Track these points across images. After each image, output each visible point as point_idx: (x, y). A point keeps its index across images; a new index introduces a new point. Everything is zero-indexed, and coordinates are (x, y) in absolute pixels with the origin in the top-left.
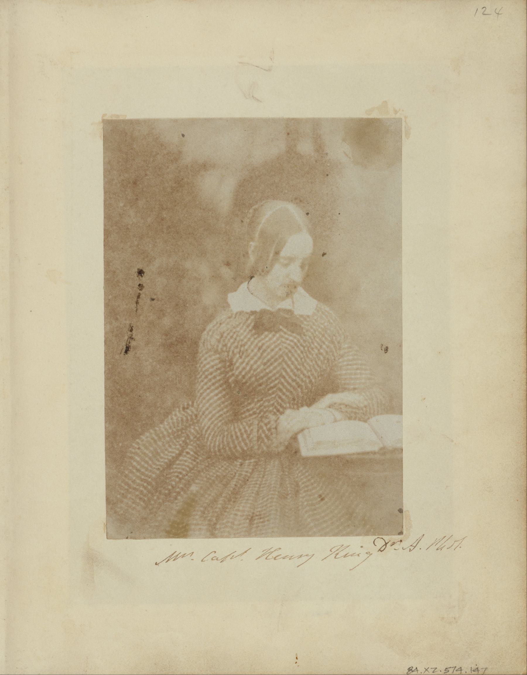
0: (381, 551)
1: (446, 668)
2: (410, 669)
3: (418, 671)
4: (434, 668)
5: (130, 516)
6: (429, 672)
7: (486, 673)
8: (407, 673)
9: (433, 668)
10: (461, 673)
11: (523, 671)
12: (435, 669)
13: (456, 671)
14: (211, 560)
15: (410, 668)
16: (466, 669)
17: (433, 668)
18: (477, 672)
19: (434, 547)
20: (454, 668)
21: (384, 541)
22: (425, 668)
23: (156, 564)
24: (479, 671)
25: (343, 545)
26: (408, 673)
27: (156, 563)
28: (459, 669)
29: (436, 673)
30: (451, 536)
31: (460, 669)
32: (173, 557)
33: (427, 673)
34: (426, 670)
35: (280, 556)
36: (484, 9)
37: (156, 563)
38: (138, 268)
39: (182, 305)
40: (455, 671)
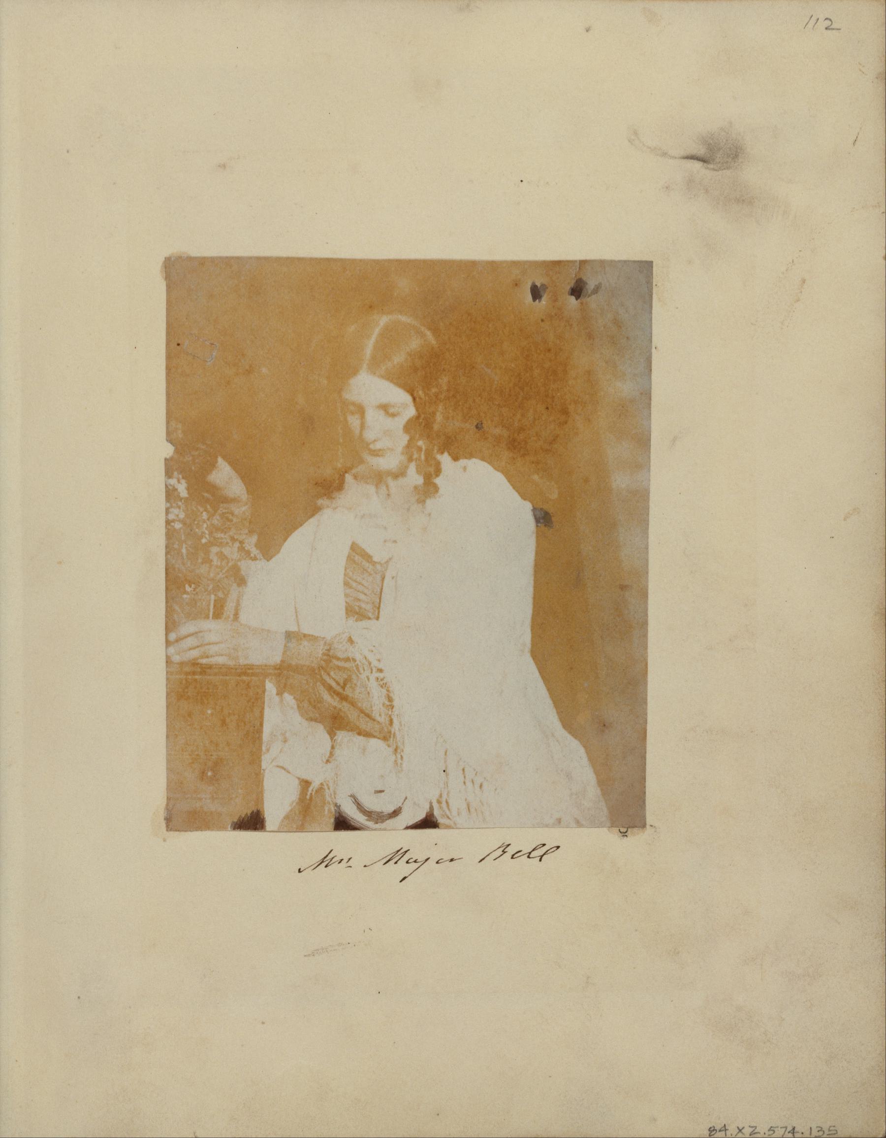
1: (771, 1127)
2: (712, 1130)
7: (784, 1137)
8: (710, 1136)
10: (726, 1135)
15: (710, 1128)
16: (763, 1129)
21: (543, 858)
22: (738, 1128)
23: (300, 871)
27: (300, 869)
28: (722, 1128)
32: (326, 861)
33: (740, 1135)
34: (740, 1131)
35: (385, 862)
37: (300, 869)
38: (575, 300)
40: (787, 1132)
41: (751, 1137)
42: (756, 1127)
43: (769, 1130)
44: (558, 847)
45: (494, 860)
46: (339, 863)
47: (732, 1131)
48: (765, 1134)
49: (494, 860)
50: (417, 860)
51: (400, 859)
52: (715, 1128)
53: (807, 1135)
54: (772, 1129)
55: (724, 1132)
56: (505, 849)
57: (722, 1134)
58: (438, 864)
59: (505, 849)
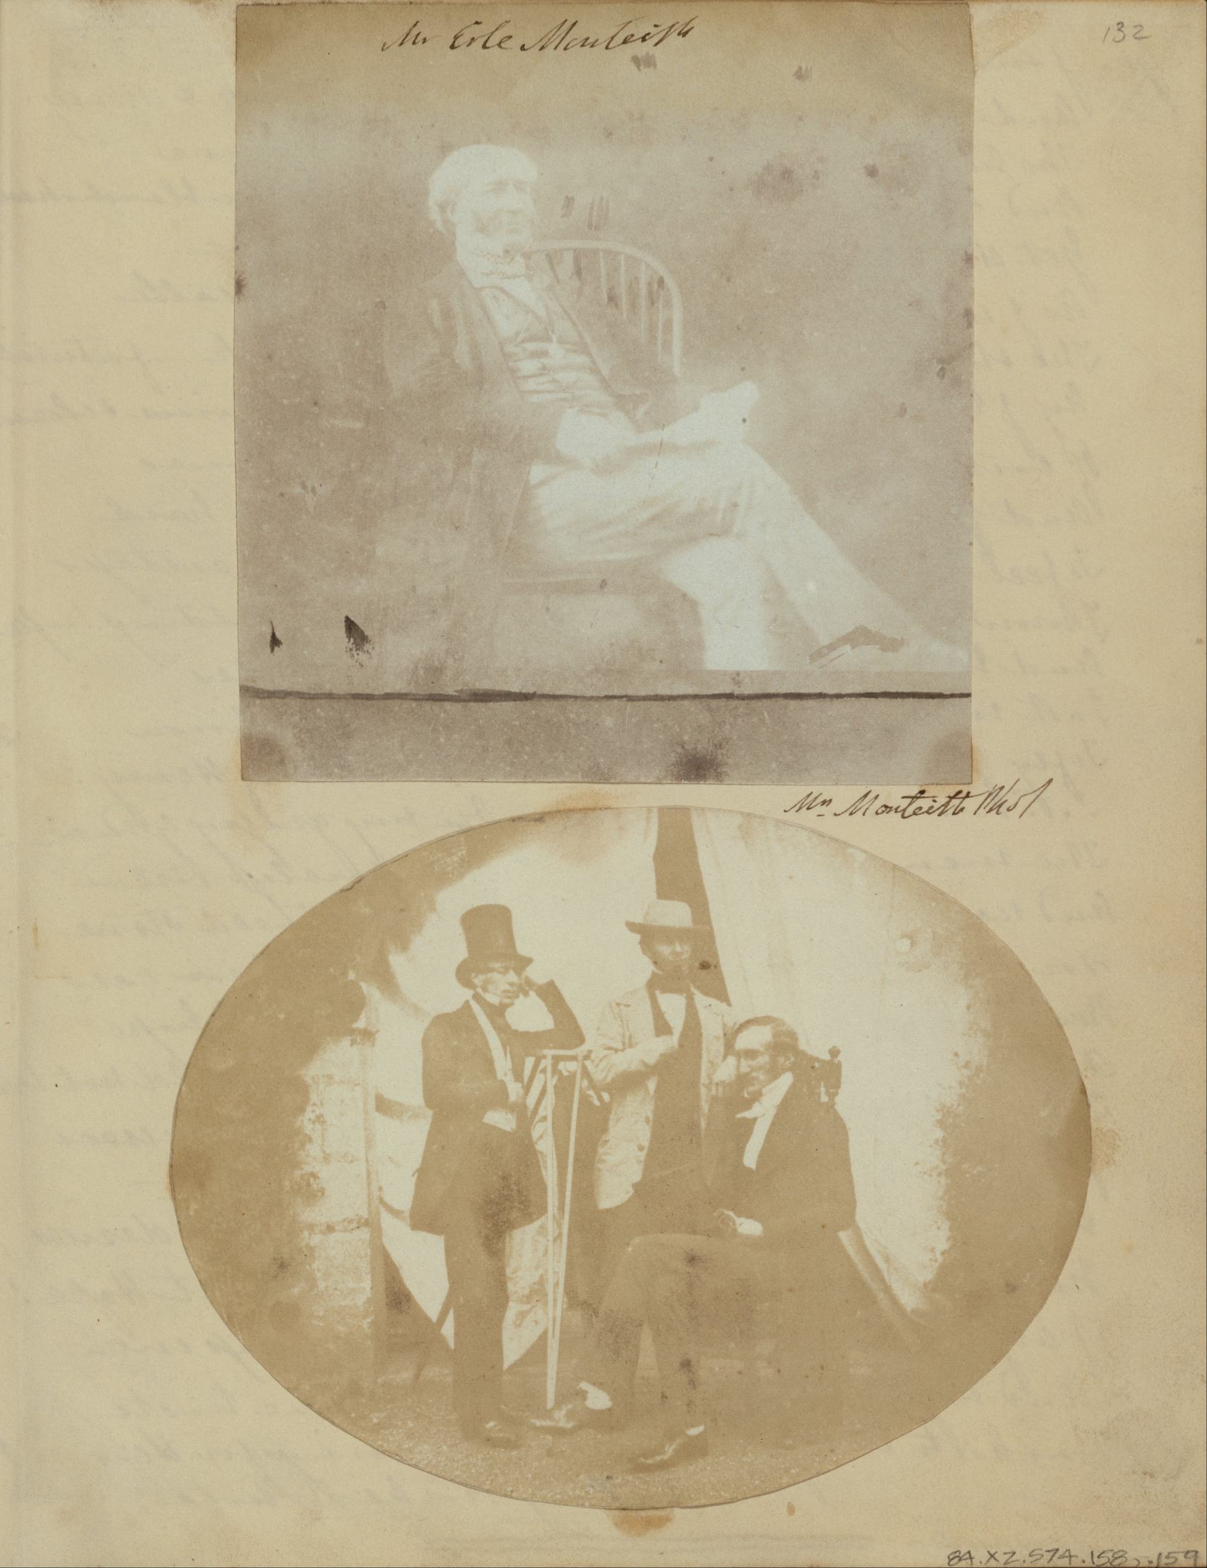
3: (974, 1560)
4: (1009, 1553)
5: (343, 387)
8: (949, 1564)
9: (1007, 1553)
10: (1070, 1563)
11: (1205, 1565)
12: (1011, 1554)
13: (1098, 1557)
17: (1007, 1553)
18: (1067, 1560)
20: (1052, 1554)
22: (989, 1552)
26: (952, 1563)
29: (1011, 1564)
31: (1067, 1554)
33: (993, 1563)
34: (992, 1556)
36: (1138, 29)
39: (542, 746)
41: (1006, 1566)
42: (1126, 1553)
43: (1030, 1555)
45: (1019, 780)
46: (468, 45)
47: (980, 1557)
48: (1024, 1561)
49: (1019, 780)
50: (524, 45)
52: (1126, 1556)
54: (1171, 1555)
56: (609, 43)
57: (963, 1564)
59: (609, 43)
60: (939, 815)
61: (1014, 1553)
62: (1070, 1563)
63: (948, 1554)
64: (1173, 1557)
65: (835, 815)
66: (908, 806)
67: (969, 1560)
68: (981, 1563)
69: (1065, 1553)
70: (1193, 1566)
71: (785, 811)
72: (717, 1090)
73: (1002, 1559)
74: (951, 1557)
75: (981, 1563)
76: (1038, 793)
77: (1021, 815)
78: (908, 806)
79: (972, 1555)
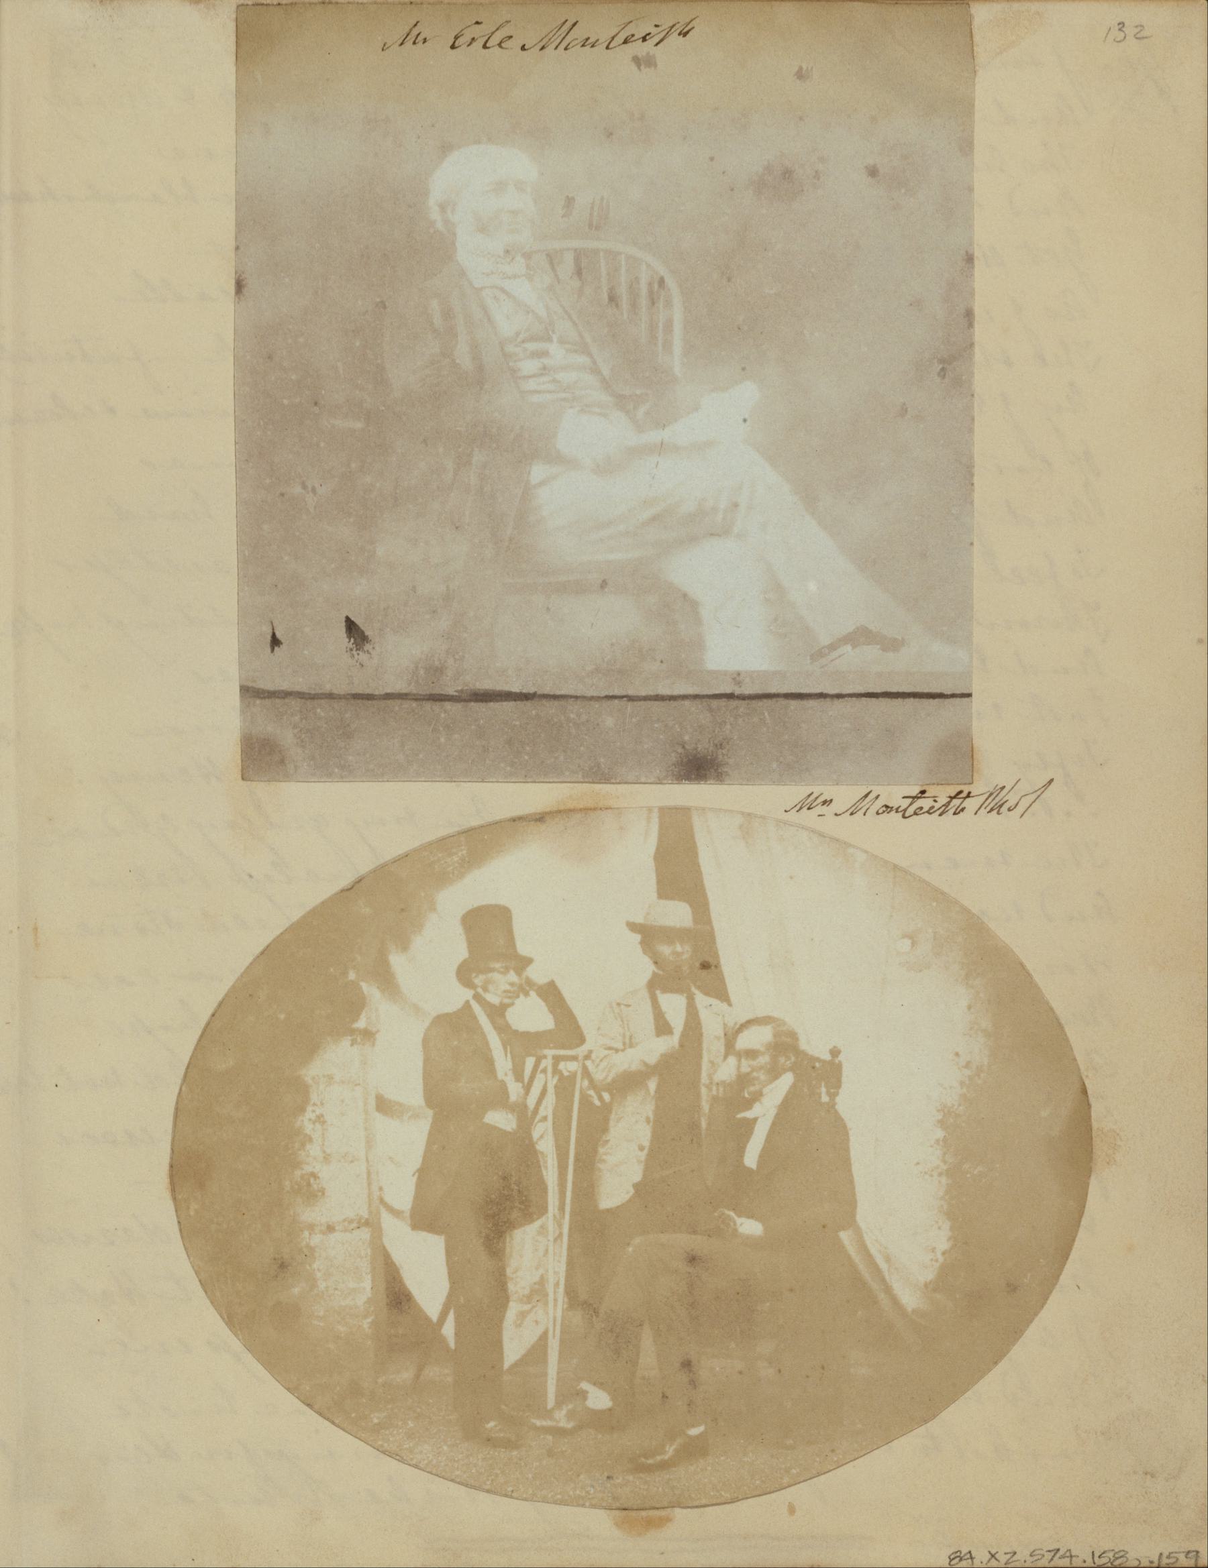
0: (957, 814)
3: (975, 1560)
6: (998, 1561)
8: (949, 1564)
9: (1008, 1553)
10: (1071, 1563)
11: (1206, 1565)
14: (520, 49)
17: (1008, 1553)
18: (1068, 1560)
19: (933, 799)
20: (1052, 1554)
21: (1023, 799)
22: (990, 1552)
24: (974, 1558)
25: (566, 49)
29: (1012, 1564)
30: (560, 23)
31: (1068, 1554)
33: (994, 1563)
34: (993, 1556)
41: (1007, 1566)
42: (1127, 1553)
43: (1031, 1555)
44: (511, 37)
45: (1019, 780)
47: (981, 1557)
48: (1025, 1561)
50: (524, 45)
51: (560, 43)
52: (1127, 1556)
53: (1089, 1564)
54: (1172, 1555)
55: (1068, 1559)
57: (964, 1564)
58: (454, 50)
60: (940, 815)
61: (1015, 1553)
62: (1071, 1563)
63: (949, 1554)
64: (1174, 1557)
65: (836, 815)
66: (909, 806)
67: (970, 1560)
68: (982, 1563)
69: (1065, 1553)
70: (1194, 1566)
71: (786, 811)
72: (718, 1090)
73: (1003, 1559)
74: (952, 1557)
75: (982, 1563)
76: (1039, 793)
77: (1022, 815)
78: (909, 806)
79: (973, 1555)
